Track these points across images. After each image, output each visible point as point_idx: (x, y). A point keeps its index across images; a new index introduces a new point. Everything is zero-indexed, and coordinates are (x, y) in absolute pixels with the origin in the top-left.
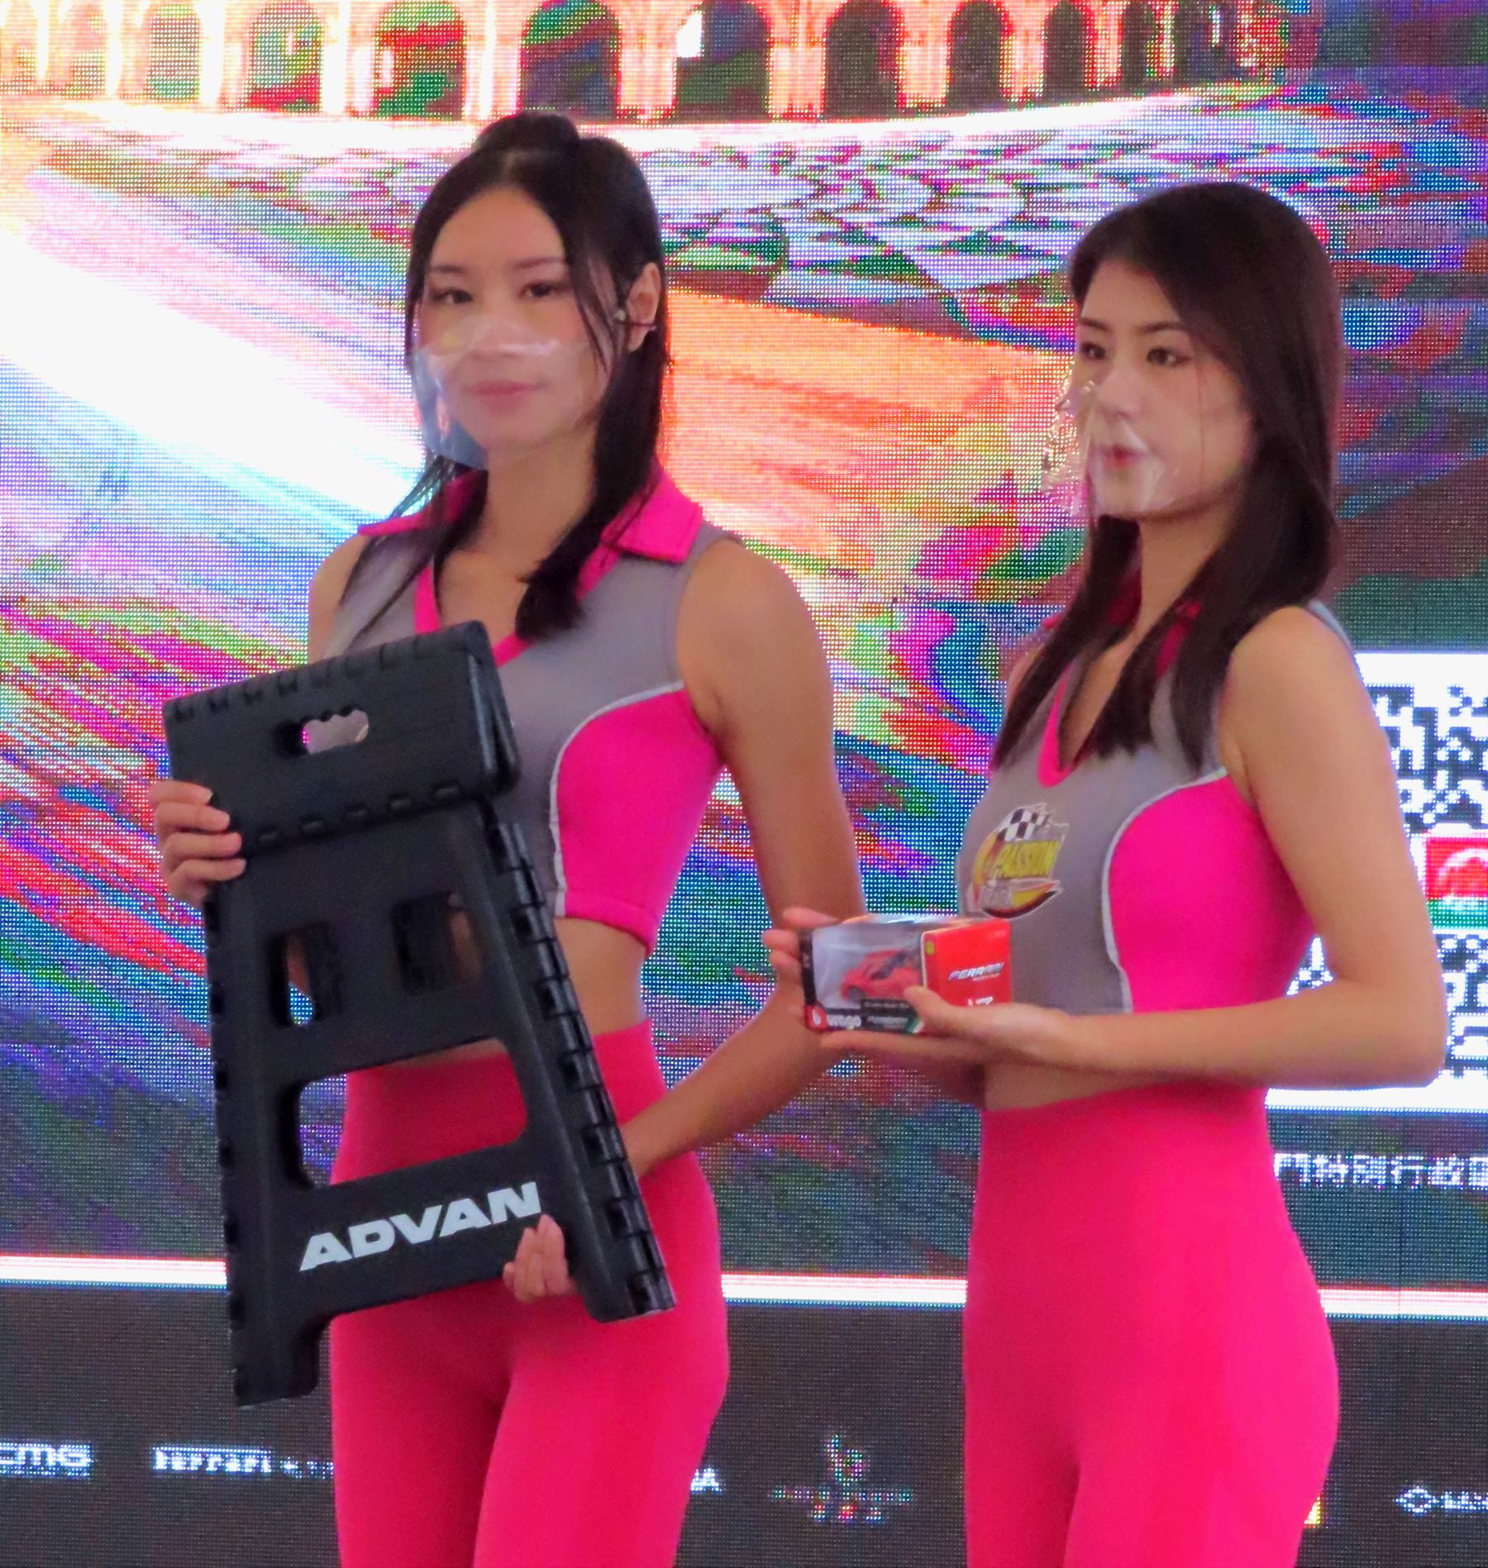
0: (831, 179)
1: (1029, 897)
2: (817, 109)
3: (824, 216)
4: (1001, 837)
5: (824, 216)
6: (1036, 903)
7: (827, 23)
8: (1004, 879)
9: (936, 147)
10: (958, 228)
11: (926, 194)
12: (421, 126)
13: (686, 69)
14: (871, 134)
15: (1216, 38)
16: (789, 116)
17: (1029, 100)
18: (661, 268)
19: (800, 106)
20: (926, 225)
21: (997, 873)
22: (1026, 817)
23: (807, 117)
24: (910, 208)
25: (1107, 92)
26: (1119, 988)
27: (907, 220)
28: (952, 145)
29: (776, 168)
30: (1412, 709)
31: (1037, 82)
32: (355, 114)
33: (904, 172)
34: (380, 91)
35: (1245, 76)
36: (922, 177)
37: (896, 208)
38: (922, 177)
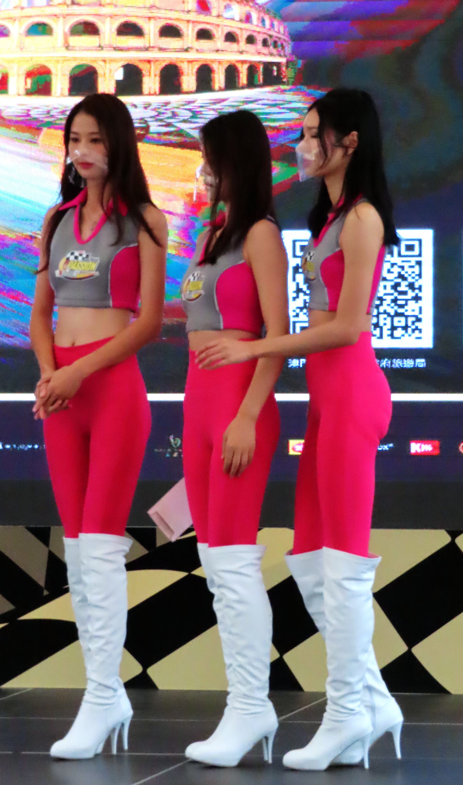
0: (162, 110)
1: (197, 295)
2: (158, 93)
3: (161, 120)
4: (189, 281)
5: (161, 120)
6: (197, 298)
7: (20, 346)
8: (190, 291)
9: (193, 102)
10: (258, 104)
11: (191, 114)
12: (38, 98)
13: (118, 82)
14: (174, 99)
15: (275, 73)
16: (150, 94)
17: (221, 90)
18: (44, 7)
19: (152, 92)
20: (191, 122)
21: (189, 290)
22: (195, 275)
23: (155, 94)
24: (186, 118)
25: (243, 88)
26: (219, 317)
27: (185, 121)
28: (198, 102)
29: (146, 108)
30: (397, 296)
31: (223, 85)
32: (19, 95)
33: (186, 109)
34: (26, 89)
35: (283, 83)
36: (190, 110)
37: (182, 118)
38: (190, 110)
